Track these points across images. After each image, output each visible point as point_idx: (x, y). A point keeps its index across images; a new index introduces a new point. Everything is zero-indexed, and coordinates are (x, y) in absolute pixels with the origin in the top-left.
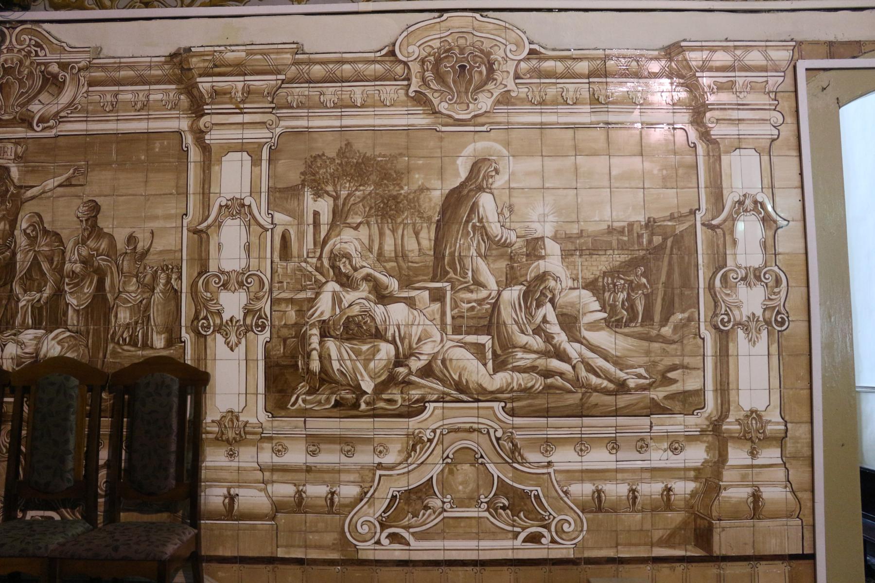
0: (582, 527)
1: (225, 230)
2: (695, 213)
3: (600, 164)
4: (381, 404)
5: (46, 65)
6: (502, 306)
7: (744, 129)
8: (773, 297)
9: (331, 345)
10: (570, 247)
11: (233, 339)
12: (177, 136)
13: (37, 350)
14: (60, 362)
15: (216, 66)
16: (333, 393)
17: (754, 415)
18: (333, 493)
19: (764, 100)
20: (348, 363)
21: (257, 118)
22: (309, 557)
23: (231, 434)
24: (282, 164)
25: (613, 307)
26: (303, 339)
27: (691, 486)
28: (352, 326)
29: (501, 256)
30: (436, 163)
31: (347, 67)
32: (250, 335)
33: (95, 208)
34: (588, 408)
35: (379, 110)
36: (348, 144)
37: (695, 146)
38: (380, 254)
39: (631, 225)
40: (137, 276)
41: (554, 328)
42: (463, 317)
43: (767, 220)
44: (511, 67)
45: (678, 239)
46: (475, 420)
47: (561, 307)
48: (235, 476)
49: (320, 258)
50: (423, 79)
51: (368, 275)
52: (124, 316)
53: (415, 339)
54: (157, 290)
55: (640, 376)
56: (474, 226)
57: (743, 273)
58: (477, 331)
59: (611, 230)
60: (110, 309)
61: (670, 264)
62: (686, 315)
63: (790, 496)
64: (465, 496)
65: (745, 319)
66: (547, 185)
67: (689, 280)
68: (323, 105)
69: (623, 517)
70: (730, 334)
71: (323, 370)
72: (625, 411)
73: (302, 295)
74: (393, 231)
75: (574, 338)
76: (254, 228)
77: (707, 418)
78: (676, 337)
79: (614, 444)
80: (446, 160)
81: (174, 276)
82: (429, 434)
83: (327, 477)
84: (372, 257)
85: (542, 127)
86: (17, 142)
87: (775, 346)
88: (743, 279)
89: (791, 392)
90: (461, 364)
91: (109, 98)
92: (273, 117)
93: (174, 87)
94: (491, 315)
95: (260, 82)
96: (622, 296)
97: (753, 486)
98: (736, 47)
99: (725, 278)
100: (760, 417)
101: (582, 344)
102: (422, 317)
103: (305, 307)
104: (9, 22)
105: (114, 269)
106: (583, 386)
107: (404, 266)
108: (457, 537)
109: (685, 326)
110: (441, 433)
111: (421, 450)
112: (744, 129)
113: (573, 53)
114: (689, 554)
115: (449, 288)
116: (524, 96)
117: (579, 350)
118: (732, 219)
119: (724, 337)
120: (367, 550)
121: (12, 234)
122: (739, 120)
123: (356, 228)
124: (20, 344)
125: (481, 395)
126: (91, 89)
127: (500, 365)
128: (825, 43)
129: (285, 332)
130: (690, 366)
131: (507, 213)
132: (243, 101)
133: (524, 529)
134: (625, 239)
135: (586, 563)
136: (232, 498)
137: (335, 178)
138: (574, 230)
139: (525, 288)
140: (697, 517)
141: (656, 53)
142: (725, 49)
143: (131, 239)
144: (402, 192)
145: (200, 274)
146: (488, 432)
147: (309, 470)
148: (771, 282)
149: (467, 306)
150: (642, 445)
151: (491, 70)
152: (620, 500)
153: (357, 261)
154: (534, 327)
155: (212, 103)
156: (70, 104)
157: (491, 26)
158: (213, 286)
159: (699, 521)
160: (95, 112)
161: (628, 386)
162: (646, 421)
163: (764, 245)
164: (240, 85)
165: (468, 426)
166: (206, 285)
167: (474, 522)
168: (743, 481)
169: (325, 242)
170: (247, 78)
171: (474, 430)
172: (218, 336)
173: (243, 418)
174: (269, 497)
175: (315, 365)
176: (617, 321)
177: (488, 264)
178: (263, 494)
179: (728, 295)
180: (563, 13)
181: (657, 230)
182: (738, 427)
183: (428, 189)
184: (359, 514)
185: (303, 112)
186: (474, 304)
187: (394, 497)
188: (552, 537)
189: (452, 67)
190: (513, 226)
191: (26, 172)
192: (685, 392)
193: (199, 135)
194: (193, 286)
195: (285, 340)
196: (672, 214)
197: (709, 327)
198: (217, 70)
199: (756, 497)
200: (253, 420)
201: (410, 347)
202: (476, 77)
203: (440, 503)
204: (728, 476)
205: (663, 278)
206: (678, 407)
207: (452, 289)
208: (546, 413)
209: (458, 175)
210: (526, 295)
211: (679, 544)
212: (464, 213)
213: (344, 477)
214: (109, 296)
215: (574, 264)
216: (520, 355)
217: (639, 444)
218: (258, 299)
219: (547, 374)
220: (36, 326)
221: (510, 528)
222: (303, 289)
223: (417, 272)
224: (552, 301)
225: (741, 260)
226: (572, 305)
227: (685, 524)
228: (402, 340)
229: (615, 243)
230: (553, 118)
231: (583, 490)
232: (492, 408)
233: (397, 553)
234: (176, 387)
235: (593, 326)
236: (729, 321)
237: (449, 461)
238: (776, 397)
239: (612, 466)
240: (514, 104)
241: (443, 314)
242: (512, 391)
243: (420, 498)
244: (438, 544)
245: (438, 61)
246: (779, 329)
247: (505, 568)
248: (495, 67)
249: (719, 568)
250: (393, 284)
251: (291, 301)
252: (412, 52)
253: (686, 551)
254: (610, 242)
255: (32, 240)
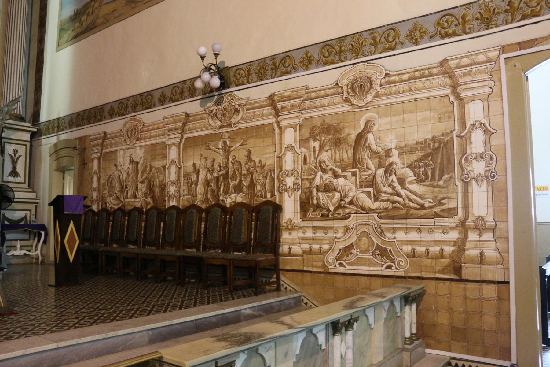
0: (407, 264)
1: (287, 156)
2: (453, 132)
3: (413, 115)
4: (336, 215)
5: (235, 105)
6: (377, 177)
7: (476, 92)
8: (489, 165)
9: (320, 194)
10: (402, 151)
11: (290, 194)
12: (272, 124)
13: (235, 200)
14: (241, 204)
15: (282, 98)
16: (321, 211)
17: (480, 218)
18: (321, 248)
19: (485, 76)
20: (325, 200)
21: (295, 115)
22: (314, 270)
23: (290, 227)
24: (303, 130)
25: (419, 174)
26: (311, 192)
27: (452, 249)
28: (327, 187)
29: (376, 157)
30: (353, 124)
31: (323, 92)
32: (295, 192)
33: (250, 152)
34: (409, 216)
35: (334, 107)
36: (324, 121)
37: (453, 103)
38: (335, 160)
39: (426, 140)
40: (262, 174)
41: (396, 184)
42: (363, 182)
43: (486, 131)
44: (378, 82)
45: (446, 144)
46: (367, 220)
47: (398, 176)
48: (291, 241)
49: (316, 163)
50: (348, 93)
51: (331, 168)
52: (259, 188)
53: (347, 191)
54: (268, 178)
55: (430, 202)
56: (366, 147)
57: (474, 156)
58: (368, 187)
59: (417, 143)
60: (255, 186)
61: (442, 155)
62: (449, 176)
63: (498, 255)
64: (364, 249)
65: (476, 176)
66: (393, 127)
67: (450, 161)
68: (315, 107)
69: (424, 260)
70: (469, 183)
71: (318, 203)
72: (424, 217)
73: (310, 177)
74: (339, 151)
75: (404, 188)
76: (296, 154)
77: (459, 220)
78: (445, 186)
79: (419, 230)
80: (356, 122)
81: (273, 173)
82: (352, 226)
83: (319, 241)
84: (333, 161)
85: (391, 104)
86: (228, 132)
87: (491, 187)
88: (475, 159)
89: (498, 208)
90: (363, 199)
91: (252, 114)
92: (300, 114)
93: (270, 107)
94: (373, 181)
95: (296, 102)
96: (422, 170)
97: (480, 249)
98: (472, 55)
99: (466, 159)
100: (483, 219)
101: (407, 190)
102: (349, 182)
103: (311, 181)
104: (225, 93)
105: (256, 172)
106: (407, 207)
107: (343, 164)
108: (362, 265)
109: (449, 180)
110: (356, 226)
111: (349, 231)
112: (476, 92)
113: (403, 72)
114: (451, 277)
115: (358, 171)
116: (384, 93)
117: (405, 192)
118: (470, 132)
119: (466, 184)
120: (332, 269)
121: (228, 163)
122: (473, 88)
123: (327, 151)
124: (231, 198)
125: (370, 211)
126: (247, 112)
127: (376, 199)
128: (516, 43)
129: (306, 190)
130: (451, 197)
131: (378, 140)
132: (291, 110)
133: (385, 263)
134: (423, 146)
135: (409, 278)
136: (290, 249)
137: (320, 134)
138: (403, 144)
139: (385, 169)
140: (455, 262)
141: (436, 65)
142: (466, 57)
143: (260, 162)
144: (342, 136)
145: (280, 172)
146: (372, 225)
147: (313, 239)
148: (488, 158)
149: (364, 177)
150: (431, 231)
151: (371, 84)
152: (423, 253)
153: (328, 163)
154: (389, 184)
155: (282, 112)
156: (242, 118)
157: (371, 67)
158: (284, 175)
159: (455, 264)
160: (248, 119)
161: (425, 206)
162: (432, 221)
163: (485, 143)
164: (290, 104)
165: (365, 223)
166: (282, 175)
167: (367, 260)
168: (476, 246)
169: (317, 157)
170: (292, 101)
171: (367, 224)
172: (286, 193)
173: (293, 221)
174: (301, 249)
175: (315, 202)
176: (420, 180)
177: (372, 161)
178: (299, 247)
179: (468, 166)
180: (399, 55)
181: (437, 141)
182: (473, 223)
183: (350, 134)
184: (329, 255)
185: (309, 111)
186: (367, 176)
187: (340, 249)
188: (396, 267)
189: (358, 86)
190: (380, 145)
191: (232, 142)
192: (449, 208)
193: (278, 123)
194: (278, 176)
195: (306, 193)
196: (443, 133)
197: (460, 180)
198: (283, 99)
199: (482, 254)
200: (296, 222)
201: (345, 194)
202: (366, 88)
203: (356, 252)
204: (468, 245)
205: (439, 161)
206: (446, 214)
207: (359, 171)
208: (393, 218)
209: (360, 127)
210: (385, 172)
211: (447, 273)
212: (363, 142)
213: (324, 242)
214: (254, 181)
215: (403, 158)
216: (383, 195)
217: (430, 230)
218: (297, 179)
219: (394, 202)
220: (235, 192)
221: (380, 263)
222: (311, 175)
223: (347, 166)
224: (395, 173)
225: (474, 150)
226: (403, 174)
227: (449, 265)
228: (343, 191)
229: (419, 149)
230: (394, 100)
231: (408, 248)
232: (373, 216)
233: (341, 270)
234: (271, 210)
235: (411, 183)
236: (469, 177)
237: (359, 236)
238: (491, 210)
239: (419, 239)
240: (380, 97)
241: (356, 181)
242: (381, 209)
243: (349, 250)
244: (355, 267)
245: (353, 84)
246: (492, 179)
247: (379, 278)
248: (373, 83)
249: (465, 284)
250: (339, 171)
251: (307, 179)
252: (344, 82)
253: (450, 276)
254: (417, 148)
255: (233, 164)
